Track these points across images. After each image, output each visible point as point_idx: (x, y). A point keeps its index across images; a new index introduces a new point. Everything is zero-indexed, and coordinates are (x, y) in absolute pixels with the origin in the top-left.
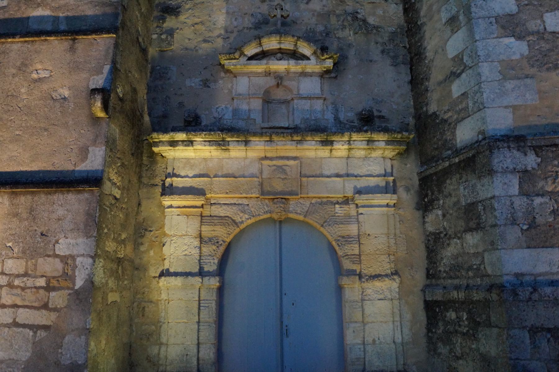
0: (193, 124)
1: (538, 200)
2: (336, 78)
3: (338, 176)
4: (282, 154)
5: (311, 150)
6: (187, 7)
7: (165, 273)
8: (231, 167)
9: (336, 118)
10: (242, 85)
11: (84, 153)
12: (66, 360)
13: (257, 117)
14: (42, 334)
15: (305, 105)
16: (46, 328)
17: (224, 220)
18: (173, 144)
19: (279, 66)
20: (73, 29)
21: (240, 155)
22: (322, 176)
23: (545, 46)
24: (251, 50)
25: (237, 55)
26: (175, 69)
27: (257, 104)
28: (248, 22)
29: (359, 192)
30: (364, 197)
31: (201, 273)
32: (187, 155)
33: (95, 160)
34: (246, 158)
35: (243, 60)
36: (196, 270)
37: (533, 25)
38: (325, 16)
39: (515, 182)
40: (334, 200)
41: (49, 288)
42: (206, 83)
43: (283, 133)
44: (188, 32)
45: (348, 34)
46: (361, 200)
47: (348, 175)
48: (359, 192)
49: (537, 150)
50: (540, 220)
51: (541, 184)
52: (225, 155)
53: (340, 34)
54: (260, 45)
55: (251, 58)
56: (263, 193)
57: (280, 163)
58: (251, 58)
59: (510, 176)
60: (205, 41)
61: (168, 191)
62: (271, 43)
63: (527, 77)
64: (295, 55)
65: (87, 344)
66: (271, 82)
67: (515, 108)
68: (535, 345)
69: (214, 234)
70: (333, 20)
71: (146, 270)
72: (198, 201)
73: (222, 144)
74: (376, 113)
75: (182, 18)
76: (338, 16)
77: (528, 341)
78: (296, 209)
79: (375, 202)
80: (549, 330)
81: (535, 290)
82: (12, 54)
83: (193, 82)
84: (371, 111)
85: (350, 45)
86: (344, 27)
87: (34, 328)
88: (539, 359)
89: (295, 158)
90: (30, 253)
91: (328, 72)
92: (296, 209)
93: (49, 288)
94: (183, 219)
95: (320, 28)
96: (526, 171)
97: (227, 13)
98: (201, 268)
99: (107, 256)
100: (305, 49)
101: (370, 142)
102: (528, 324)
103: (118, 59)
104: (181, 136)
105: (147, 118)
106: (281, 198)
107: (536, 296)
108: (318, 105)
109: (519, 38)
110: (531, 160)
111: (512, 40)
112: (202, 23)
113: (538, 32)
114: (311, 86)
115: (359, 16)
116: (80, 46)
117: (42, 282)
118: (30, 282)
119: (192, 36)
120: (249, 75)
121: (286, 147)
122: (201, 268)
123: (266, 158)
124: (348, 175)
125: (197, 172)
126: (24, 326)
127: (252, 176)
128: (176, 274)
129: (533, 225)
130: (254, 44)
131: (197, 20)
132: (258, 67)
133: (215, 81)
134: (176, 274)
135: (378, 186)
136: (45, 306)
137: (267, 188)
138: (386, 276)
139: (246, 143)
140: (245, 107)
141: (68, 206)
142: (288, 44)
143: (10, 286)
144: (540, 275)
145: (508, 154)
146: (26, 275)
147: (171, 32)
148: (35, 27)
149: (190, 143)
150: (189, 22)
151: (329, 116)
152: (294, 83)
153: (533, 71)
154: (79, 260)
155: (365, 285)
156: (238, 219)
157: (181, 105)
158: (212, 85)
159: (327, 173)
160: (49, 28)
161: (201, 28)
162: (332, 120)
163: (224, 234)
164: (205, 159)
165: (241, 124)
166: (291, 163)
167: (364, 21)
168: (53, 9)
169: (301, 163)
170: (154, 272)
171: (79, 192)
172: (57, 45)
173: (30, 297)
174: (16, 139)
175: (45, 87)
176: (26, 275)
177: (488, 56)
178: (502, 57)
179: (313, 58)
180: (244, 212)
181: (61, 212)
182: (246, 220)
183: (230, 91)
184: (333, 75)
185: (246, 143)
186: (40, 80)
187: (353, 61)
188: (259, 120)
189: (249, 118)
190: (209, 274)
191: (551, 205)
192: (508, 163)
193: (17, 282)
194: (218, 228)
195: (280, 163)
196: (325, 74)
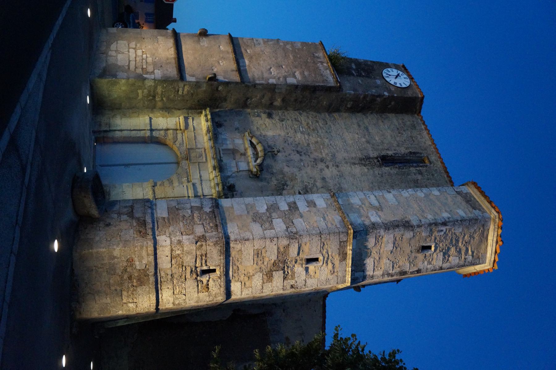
0: (217, 127)
1: (189, 211)
2: (250, 177)
3: (201, 176)
4: (208, 155)
5: (211, 163)
6: (273, 121)
7: (151, 119)
8: (199, 138)
9: (229, 177)
10: (238, 141)
11: (193, 76)
12: (117, 73)
13: (224, 147)
14: (127, 68)
15: (233, 164)
16: (129, 68)
17: (175, 139)
18: (206, 116)
19: (250, 152)
20: (240, 70)
21: (205, 141)
22: (200, 170)
23: (265, 218)
24: (254, 141)
25: (250, 135)
26: (242, 118)
27: (230, 147)
28: (270, 143)
29: (194, 185)
30: (192, 186)
31: (152, 130)
32: (202, 123)
33: (189, 78)
34: (204, 143)
35: (250, 138)
36: (153, 128)
37: (274, 215)
38: (282, 172)
39: (197, 205)
40: (189, 177)
41: (142, 69)
42: (237, 129)
43: (216, 153)
44: (260, 122)
45: (274, 182)
46: (190, 185)
47: (201, 180)
48: (194, 185)
49: (213, 212)
50: (180, 211)
51: (197, 212)
52: (204, 135)
53: (273, 179)
54: (258, 144)
55: (251, 141)
56: (189, 149)
57: (204, 155)
58: (251, 141)
59: (199, 203)
60: (258, 128)
61: (186, 119)
62: (259, 148)
63: (248, 212)
64: (256, 156)
65: (123, 79)
66: (242, 151)
67: (232, 207)
68: (126, 207)
69: (169, 135)
70: (281, 176)
71: (152, 113)
72: (182, 127)
73: (208, 131)
74: (235, 193)
75: (267, 120)
76: (283, 178)
77: (128, 205)
78: (184, 163)
79: (190, 191)
80: (132, 211)
81: (150, 207)
82: (228, 55)
83: (237, 124)
84: (235, 191)
85: (268, 183)
86: (277, 180)
87: (129, 66)
88: (120, 208)
89: (206, 159)
90: (155, 64)
91: (251, 172)
92: (184, 163)
93: (142, 69)
94: (174, 123)
95: (275, 171)
96: (202, 208)
97: (274, 136)
98: (154, 130)
99: (156, 87)
100: (259, 161)
101: (218, 184)
102: (135, 205)
103: (232, 85)
104: (209, 117)
105: (217, 110)
106: (187, 158)
107: (146, 207)
108: (235, 169)
109: (267, 210)
110: (207, 209)
111: (266, 208)
112: (266, 127)
113: (271, 216)
114: (243, 166)
115: (285, 187)
116: (234, 73)
117: (144, 67)
118: (144, 64)
119: (259, 124)
120: (244, 143)
121: (210, 154)
122: (154, 130)
123: (205, 150)
124: (201, 180)
125: (195, 127)
126: (129, 63)
127: (196, 146)
128: (151, 121)
129: (178, 209)
130: (257, 141)
131: (267, 125)
132: (247, 145)
133: (239, 133)
134: (151, 121)
135: (197, 192)
136: (136, 68)
137: (191, 151)
138: (155, 196)
139: (210, 140)
140: (228, 142)
141: (173, 72)
142: (260, 154)
143: (143, 59)
144: (156, 211)
145: (209, 203)
146: (147, 63)
147: (259, 116)
148: (241, 61)
149: (207, 121)
150: (266, 123)
151: (229, 174)
152: (243, 160)
153: (251, 213)
154: (153, 75)
155: (150, 188)
156: (177, 143)
157: (226, 121)
158: (237, 131)
159: (201, 172)
160: (241, 64)
161: (264, 127)
162: (227, 175)
163: (169, 142)
164: (201, 129)
165: (220, 141)
166: (204, 159)
167: (283, 189)
168: (249, 66)
169: (205, 162)
170: (151, 115)
171: (178, 75)
172: (234, 66)
173: (139, 64)
174: (195, 58)
175: (216, 64)
176: (147, 63)
177: (257, 200)
178: (257, 205)
179: (256, 164)
180: (180, 144)
181: (170, 70)
182: (175, 148)
183: (235, 138)
184: (251, 176)
185: (210, 140)
186: (219, 63)
187: (260, 184)
188: (223, 148)
189: (223, 144)
190: (151, 133)
191: (187, 215)
192: (205, 203)
193: (144, 61)
194: (172, 135)
195: (204, 155)
196: (250, 171)
